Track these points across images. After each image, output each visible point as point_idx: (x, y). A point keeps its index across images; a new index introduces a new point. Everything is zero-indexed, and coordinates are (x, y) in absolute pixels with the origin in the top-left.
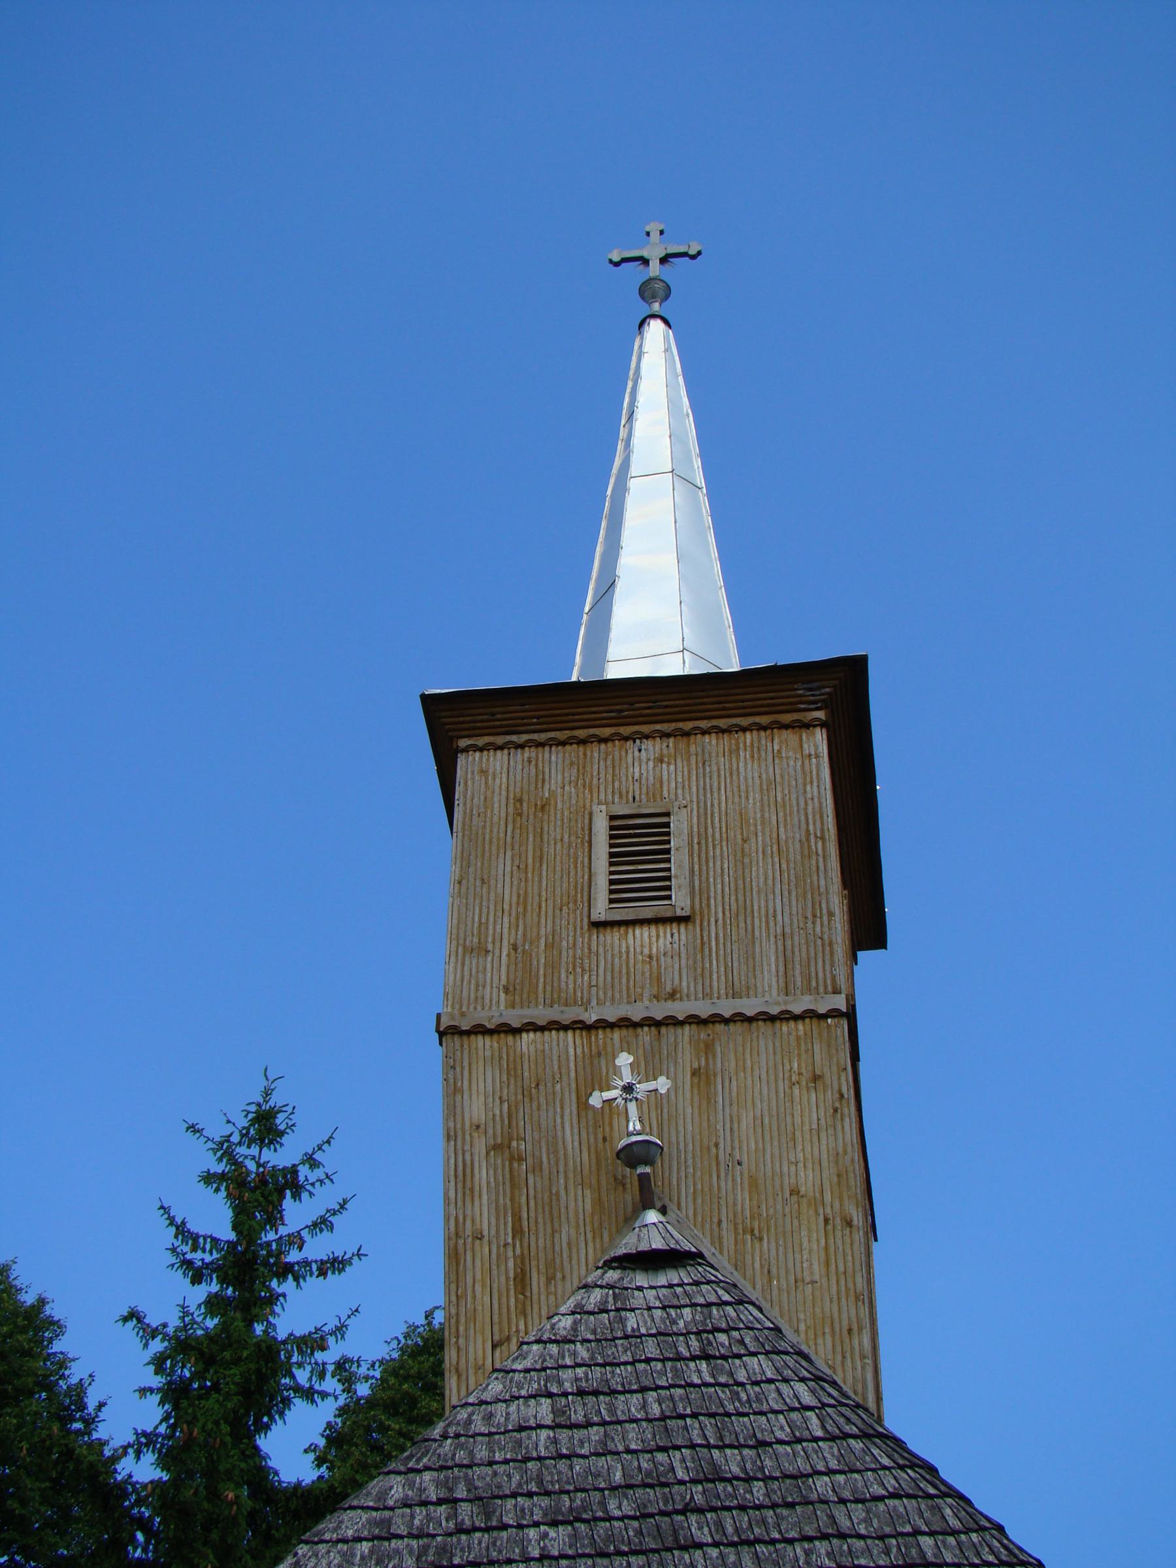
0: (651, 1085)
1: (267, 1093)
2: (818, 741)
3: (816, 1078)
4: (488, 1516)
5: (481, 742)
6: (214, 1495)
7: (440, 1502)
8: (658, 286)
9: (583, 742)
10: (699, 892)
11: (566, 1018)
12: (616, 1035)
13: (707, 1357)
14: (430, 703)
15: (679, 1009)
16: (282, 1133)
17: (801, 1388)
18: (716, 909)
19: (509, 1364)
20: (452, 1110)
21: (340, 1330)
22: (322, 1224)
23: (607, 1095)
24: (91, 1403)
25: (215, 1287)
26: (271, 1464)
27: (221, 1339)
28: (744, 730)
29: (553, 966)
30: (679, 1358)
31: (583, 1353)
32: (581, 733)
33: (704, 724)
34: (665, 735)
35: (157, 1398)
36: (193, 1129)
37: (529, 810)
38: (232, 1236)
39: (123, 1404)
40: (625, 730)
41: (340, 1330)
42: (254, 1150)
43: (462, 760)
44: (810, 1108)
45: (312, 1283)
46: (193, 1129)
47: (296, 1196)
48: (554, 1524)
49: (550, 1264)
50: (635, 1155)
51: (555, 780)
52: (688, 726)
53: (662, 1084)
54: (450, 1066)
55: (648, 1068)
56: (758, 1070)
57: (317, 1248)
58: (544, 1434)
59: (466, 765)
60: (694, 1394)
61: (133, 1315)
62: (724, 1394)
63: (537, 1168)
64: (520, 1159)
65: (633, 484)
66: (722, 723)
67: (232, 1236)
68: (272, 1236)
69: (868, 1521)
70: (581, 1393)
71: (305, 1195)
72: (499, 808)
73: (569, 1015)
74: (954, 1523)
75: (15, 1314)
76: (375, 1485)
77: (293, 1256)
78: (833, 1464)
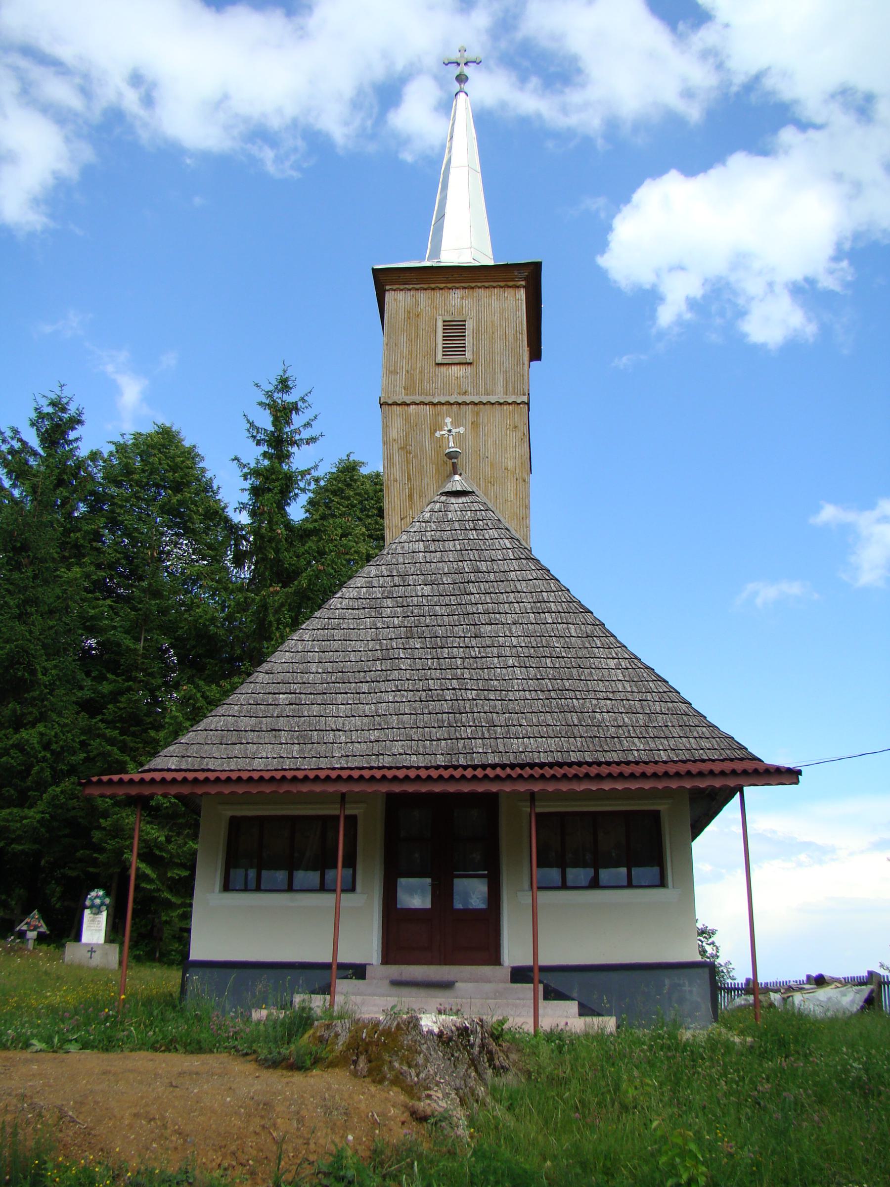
0: (457, 430)
1: (285, 371)
2: (522, 294)
3: (515, 427)
4: (404, 581)
5: (395, 287)
6: (272, 530)
7: (388, 576)
8: (463, 77)
9: (433, 289)
10: (476, 353)
11: (426, 401)
12: (445, 407)
13: (476, 530)
14: (375, 272)
15: (468, 399)
16: (291, 388)
17: (506, 541)
19: (408, 529)
20: (385, 433)
21: (316, 467)
22: (308, 425)
23: (442, 433)
24: (215, 488)
25: (266, 448)
26: (291, 517)
27: (271, 470)
28: (494, 287)
29: (422, 380)
30: (466, 530)
31: (434, 526)
32: (433, 286)
33: (479, 284)
34: (464, 288)
35: (248, 492)
36: (257, 385)
37: (413, 316)
38: (273, 429)
39: (233, 494)
40: (449, 285)
41: (316, 467)
42: (280, 395)
43: (387, 294)
44: (512, 439)
45: (304, 447)
46: (257, 385)
47: (297, 413)
48: (426, 585)
49: (421, 491)
50: (451, 456)
51: (422, 305)
52: (473, 285)
53: (462, 430)
54: (384, 417)
55: (456, 424)
56: (496, 423)
57: (306, 434)
58: (421, 554)
59: (389, 297)
60: (471, 542)
61: (236, 459)
62: (481, 543)
63: (416, 456)
64: (410, 453)
65: (451, 170)
66: (486, 284)
67: (273, 429)
68: (288, 429)
69: (527, 587)
70: (433, 540)
71: (300, 413)
72: (402, 315)
73: (427, 399)
74: (554, 589)
75: (183, 453)
76: (366, 569)
77: (297, 437)
78: (516, 568)
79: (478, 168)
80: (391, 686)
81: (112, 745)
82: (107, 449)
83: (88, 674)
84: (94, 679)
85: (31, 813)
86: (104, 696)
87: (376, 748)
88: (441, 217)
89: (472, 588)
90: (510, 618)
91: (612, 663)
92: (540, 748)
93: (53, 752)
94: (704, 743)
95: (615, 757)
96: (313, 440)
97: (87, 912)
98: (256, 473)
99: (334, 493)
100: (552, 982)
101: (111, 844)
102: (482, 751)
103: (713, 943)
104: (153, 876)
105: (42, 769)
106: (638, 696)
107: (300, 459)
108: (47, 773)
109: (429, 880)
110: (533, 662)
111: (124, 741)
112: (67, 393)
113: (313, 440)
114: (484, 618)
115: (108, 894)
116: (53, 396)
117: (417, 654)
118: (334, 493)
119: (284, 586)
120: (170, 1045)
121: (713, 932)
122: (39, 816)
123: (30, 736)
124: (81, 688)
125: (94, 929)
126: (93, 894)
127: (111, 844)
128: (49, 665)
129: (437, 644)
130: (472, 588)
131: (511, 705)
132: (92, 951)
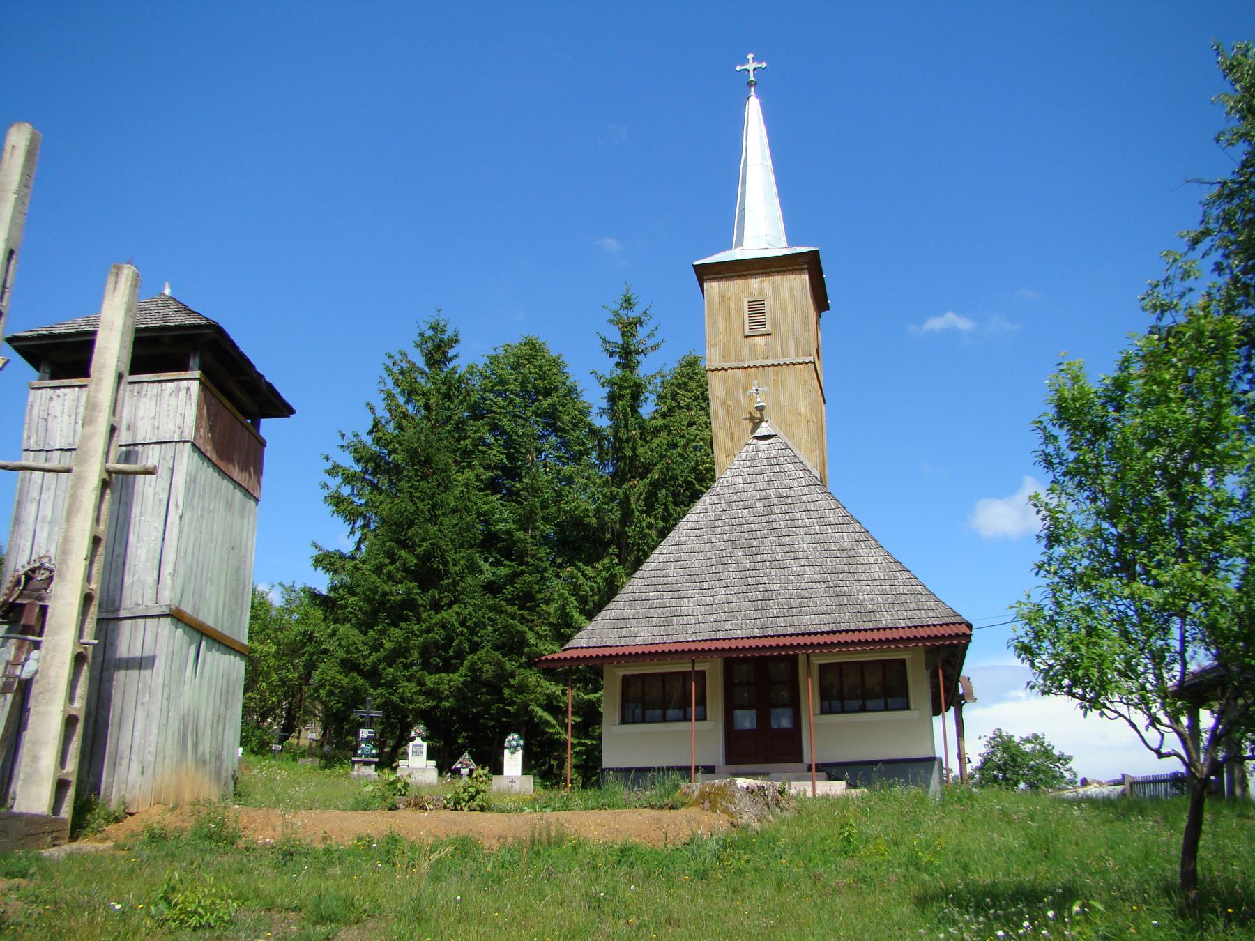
18: (778, 330)
22: (651, 335)
39: (594, 398)
47: (641, 324)
57: (650, 343)
59: (706, 285)
72: (717, 300)
79: (769, 162)
80: (723, 583)
81: (513, 618)
82: (481, 363)
83: (486, 560)
84: (492, 564)
85: (455, 676)
86: (500, 578)
87: (715, 626)
88: (743, 210)
89: (776, 509)
90: (802, 531)
91: (872, 560)
92: (821, 622)
93: (468, 627)
94: (931, 613)
95: (870, 625)
96: (657, 346)
97: (506, 751)
98: (611, 383)
99: (679, 386)
100: (831, 771)
101: (520, 699)
102: (784, 625)
103: (1070, 769)
104: (554, 722)
105: (461, 642)
106: (888, 582)
107: (646, 368)
108: (466, 646)
109: (754, 711)
110: (818, 562)
111: (522, 615)
112: (443, 318)
113: (657, 346)
114: (785, 532)
115: (521, 738)
116: (432, 321)
117: (740, 559)
118: (679, 386)
119: (642, 478)
120: (603, 807)
121: (1070, 758)
122: (462, 679)
123: (450, 615)
124: (482, 572)
125: (513, 762)
126: (510, 737)
127: (520, 699)
128: (457, 557)
129: (753, 552)
130: (776, 509)
131: (803, 593)
132: (512, 782)
